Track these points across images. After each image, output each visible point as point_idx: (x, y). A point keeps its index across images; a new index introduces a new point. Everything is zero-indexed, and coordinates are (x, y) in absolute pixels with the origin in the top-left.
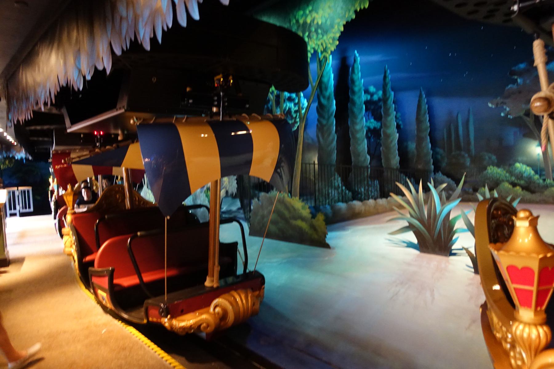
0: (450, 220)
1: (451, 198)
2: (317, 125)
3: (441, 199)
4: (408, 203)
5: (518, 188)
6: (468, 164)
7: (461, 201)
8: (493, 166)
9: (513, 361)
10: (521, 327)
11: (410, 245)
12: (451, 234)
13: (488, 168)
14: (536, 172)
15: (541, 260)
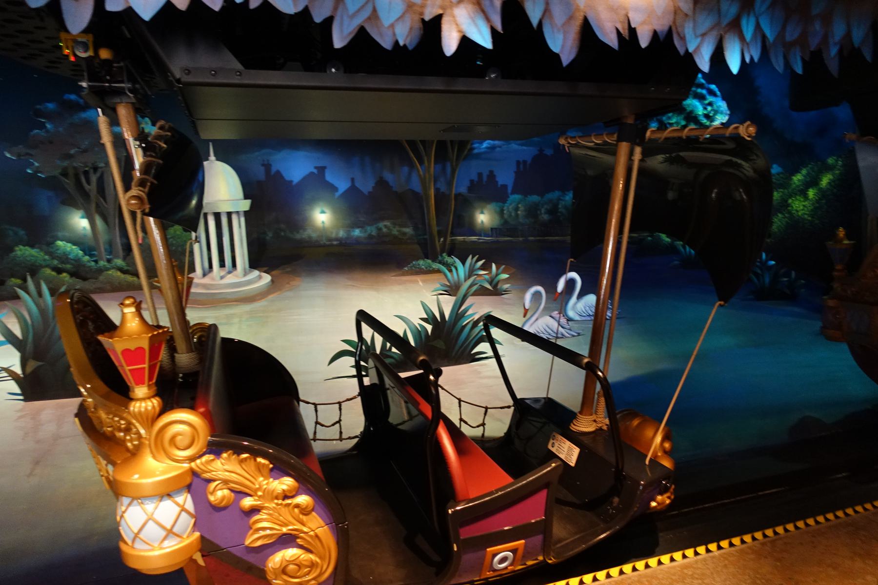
8: (24, 246)
9: (129, 444)
10: (138, 404)
15: (151, 338)
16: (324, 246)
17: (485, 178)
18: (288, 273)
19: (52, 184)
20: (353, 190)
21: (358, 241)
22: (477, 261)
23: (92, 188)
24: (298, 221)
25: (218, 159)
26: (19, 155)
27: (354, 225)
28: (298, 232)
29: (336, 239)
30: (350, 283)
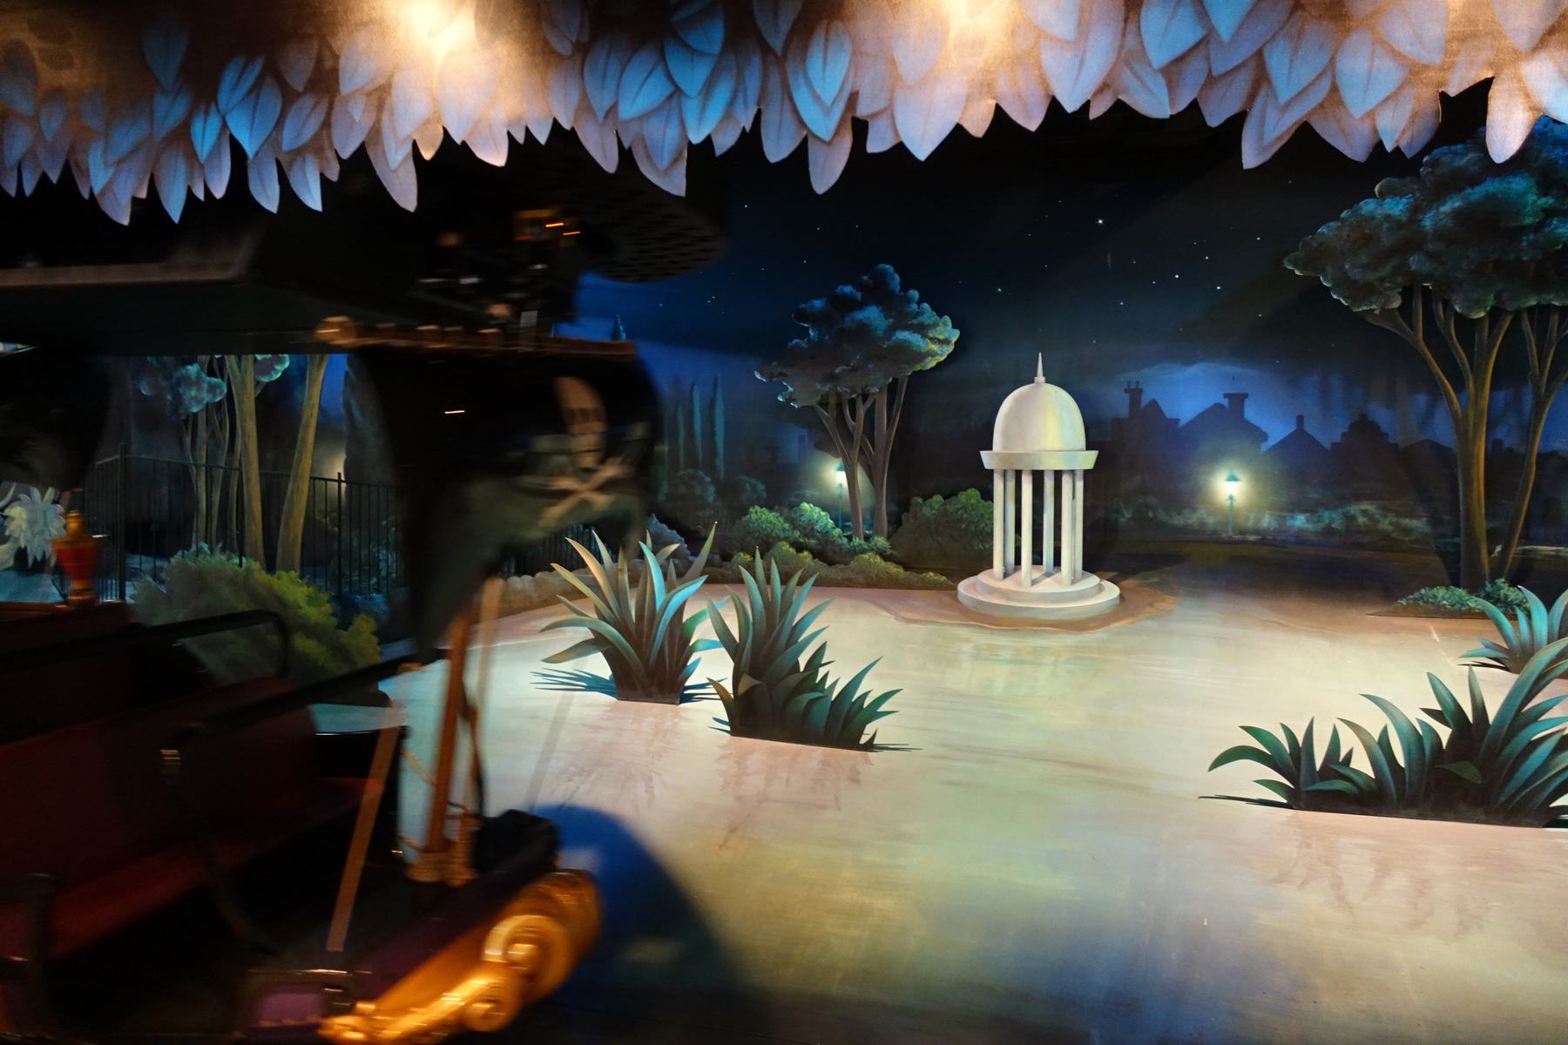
0: (684, 620)
1: (688, 575)
2: (347, 374)
3: (665, 575)
4: (594, 585)
5: (806, 553)
6: (711, 499)
7: (706, 582)
11: (594, 684)
12: (684, 655)
13: (751, 510)
14: (835, 520)
16: (1230, 542)
18: (1150, 585)
19: (806, 417)
20: (1299, 440)
21: (1300, 538)
23: (858, 426)
24: (1183, 494)
26: (771, 377)
27: (1295, 507)
29: (1256, 532)
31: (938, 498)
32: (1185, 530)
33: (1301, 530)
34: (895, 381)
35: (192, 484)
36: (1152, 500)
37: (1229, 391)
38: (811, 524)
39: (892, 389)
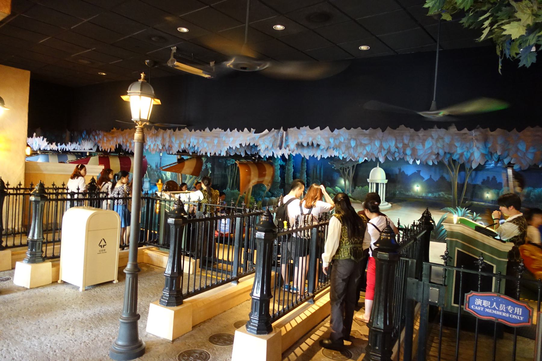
16: (417, 198)
17: (491, 179)
18: (398, 205)
19: (338, 171)
20: (430, 179)
21: (430, 198)
22: (467, 210)
23: (346, 173)
24: (408, 188)
25: (379, 167)
26: (331, 163)
27: (429, 192)
28: (408, 192)
29: (422, 196)
30: (418, 211)
31: (361, 187)
32: (408, 195)
33: (430, 197)
34: (354, 165)
35: (509, 196)
36: (402, 190)
37: (418, 170)
38: (337, 190)
39: (353, 166)
